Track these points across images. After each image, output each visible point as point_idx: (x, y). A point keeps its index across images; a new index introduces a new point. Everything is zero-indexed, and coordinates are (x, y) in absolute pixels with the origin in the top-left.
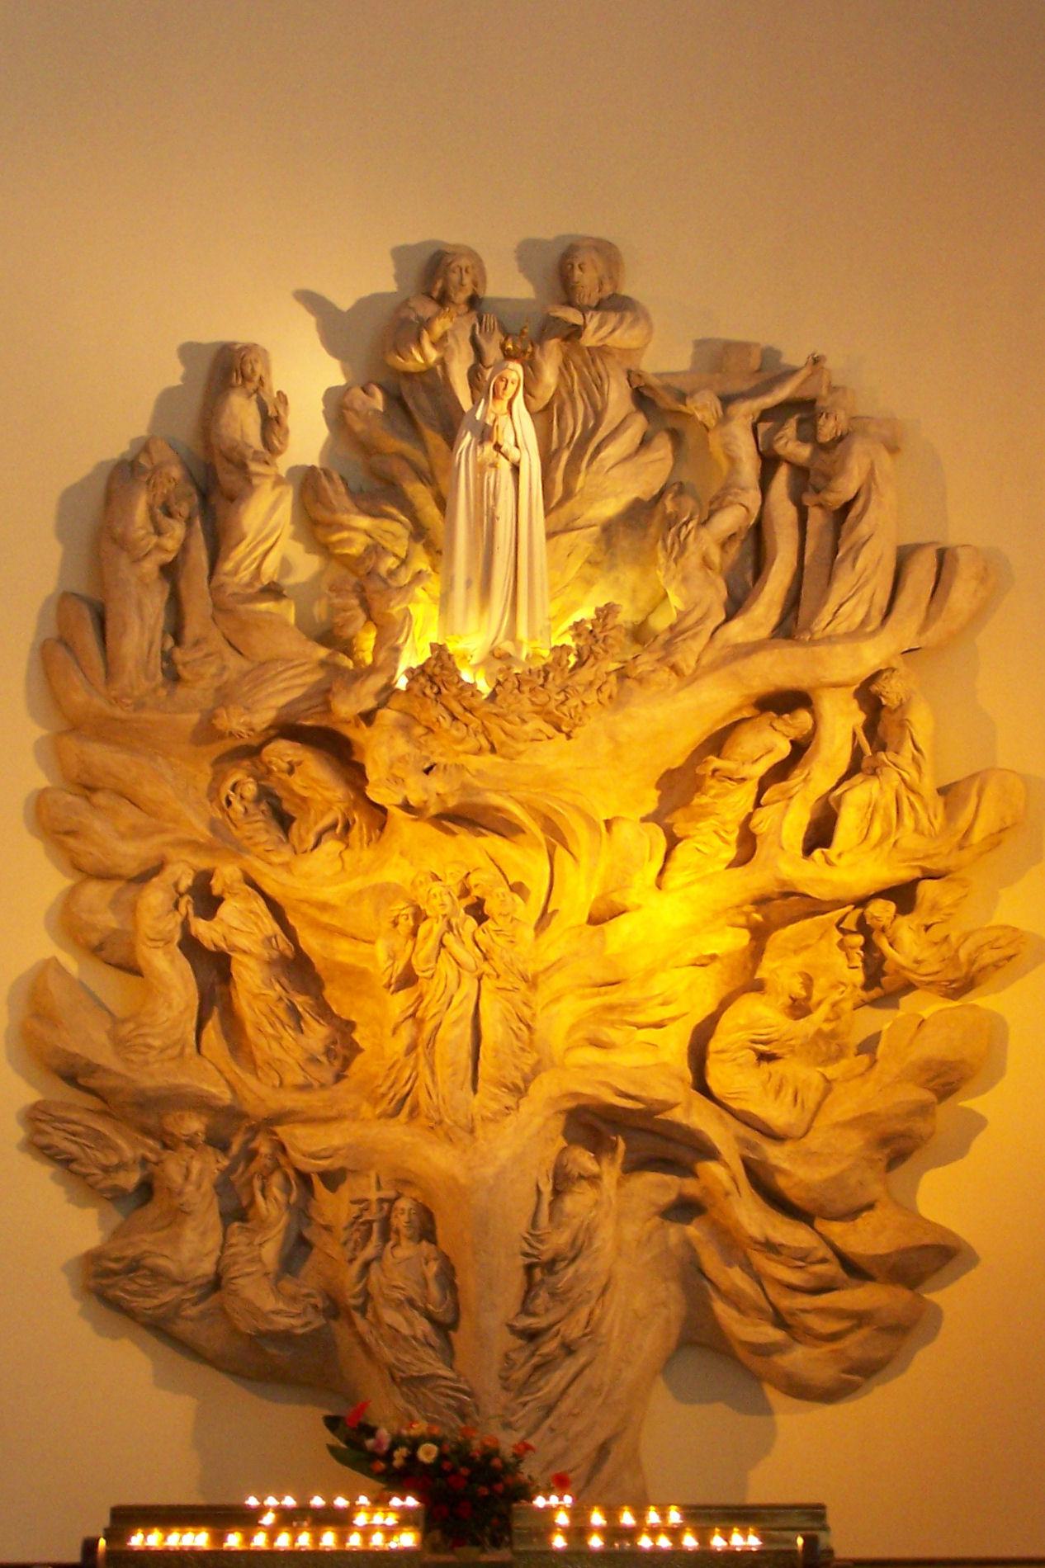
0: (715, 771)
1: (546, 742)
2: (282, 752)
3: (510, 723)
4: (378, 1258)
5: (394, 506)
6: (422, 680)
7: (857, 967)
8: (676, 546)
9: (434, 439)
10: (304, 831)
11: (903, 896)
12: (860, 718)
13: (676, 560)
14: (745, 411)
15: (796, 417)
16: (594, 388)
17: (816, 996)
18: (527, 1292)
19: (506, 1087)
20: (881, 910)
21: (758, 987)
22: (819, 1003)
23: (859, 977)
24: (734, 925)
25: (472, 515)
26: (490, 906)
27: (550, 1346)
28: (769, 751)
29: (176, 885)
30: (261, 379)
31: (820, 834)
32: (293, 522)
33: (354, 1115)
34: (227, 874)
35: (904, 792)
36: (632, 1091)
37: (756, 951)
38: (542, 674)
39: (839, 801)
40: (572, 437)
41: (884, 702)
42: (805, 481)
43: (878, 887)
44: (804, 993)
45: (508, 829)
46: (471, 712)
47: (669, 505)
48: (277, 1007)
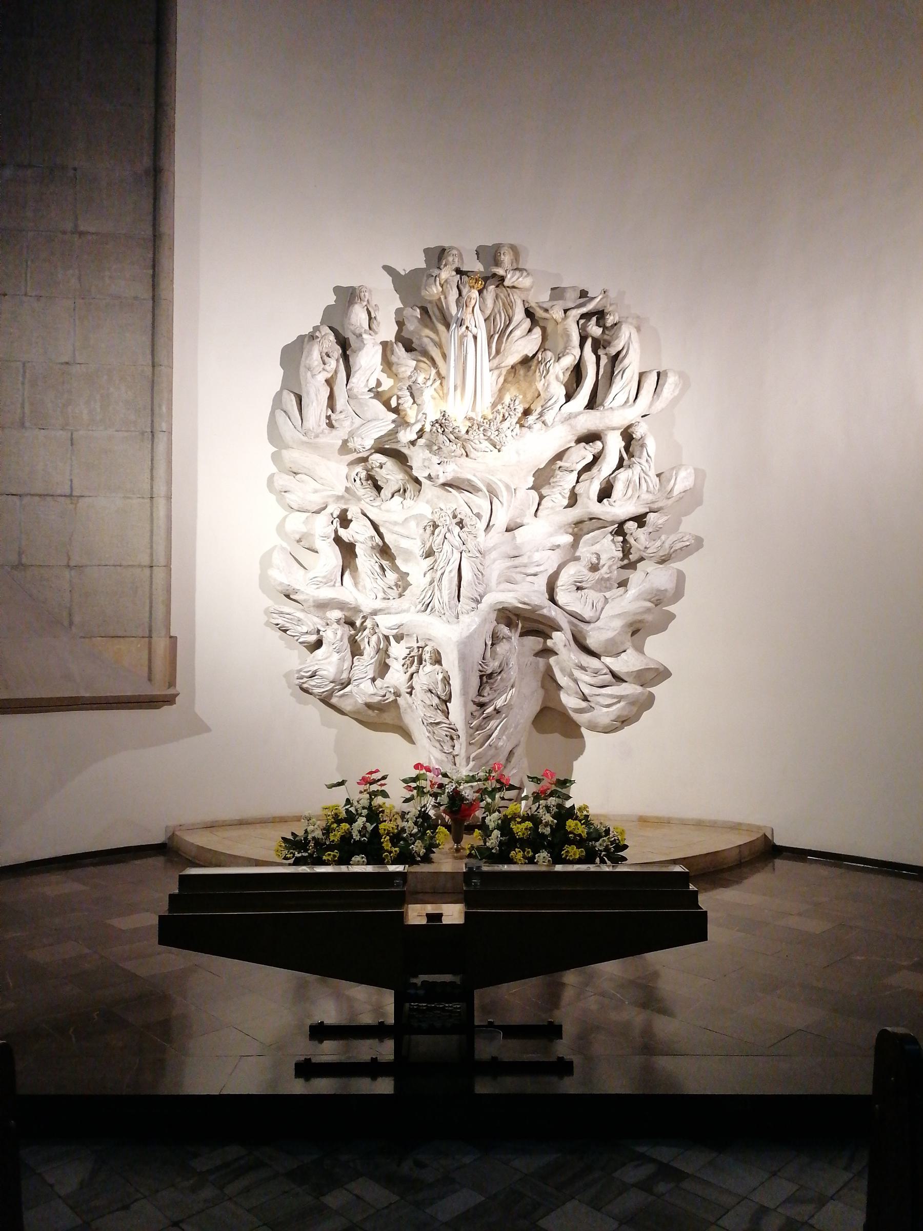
0: (560, 467)
2: (378, 458)
6: (437, 425)
8: (545, 372)
9: (441, 328)
11: (640, 520)
12: (623, 444)
14: (576, 313)
15: (596, 316)
16: (509, 306)
17: (602, 562)
19: (472, 599)
20: (631, 526)
21: (577, 559)
22: (604, 565)
23: (620, 555)
24: (567, 533)
26: (466, 521)
27: (490, 710)
29: (332, 514)
31: (605, 493)
33: (407, 611)
35: (643, 475)
36: (526, 600)
37: (575, 545)
38: (488, 423)
40: (499, 329)
41: (634, 436)
42: (597, 345)
44: (597, 562)
46: (457, 439)
47: (540, 355)
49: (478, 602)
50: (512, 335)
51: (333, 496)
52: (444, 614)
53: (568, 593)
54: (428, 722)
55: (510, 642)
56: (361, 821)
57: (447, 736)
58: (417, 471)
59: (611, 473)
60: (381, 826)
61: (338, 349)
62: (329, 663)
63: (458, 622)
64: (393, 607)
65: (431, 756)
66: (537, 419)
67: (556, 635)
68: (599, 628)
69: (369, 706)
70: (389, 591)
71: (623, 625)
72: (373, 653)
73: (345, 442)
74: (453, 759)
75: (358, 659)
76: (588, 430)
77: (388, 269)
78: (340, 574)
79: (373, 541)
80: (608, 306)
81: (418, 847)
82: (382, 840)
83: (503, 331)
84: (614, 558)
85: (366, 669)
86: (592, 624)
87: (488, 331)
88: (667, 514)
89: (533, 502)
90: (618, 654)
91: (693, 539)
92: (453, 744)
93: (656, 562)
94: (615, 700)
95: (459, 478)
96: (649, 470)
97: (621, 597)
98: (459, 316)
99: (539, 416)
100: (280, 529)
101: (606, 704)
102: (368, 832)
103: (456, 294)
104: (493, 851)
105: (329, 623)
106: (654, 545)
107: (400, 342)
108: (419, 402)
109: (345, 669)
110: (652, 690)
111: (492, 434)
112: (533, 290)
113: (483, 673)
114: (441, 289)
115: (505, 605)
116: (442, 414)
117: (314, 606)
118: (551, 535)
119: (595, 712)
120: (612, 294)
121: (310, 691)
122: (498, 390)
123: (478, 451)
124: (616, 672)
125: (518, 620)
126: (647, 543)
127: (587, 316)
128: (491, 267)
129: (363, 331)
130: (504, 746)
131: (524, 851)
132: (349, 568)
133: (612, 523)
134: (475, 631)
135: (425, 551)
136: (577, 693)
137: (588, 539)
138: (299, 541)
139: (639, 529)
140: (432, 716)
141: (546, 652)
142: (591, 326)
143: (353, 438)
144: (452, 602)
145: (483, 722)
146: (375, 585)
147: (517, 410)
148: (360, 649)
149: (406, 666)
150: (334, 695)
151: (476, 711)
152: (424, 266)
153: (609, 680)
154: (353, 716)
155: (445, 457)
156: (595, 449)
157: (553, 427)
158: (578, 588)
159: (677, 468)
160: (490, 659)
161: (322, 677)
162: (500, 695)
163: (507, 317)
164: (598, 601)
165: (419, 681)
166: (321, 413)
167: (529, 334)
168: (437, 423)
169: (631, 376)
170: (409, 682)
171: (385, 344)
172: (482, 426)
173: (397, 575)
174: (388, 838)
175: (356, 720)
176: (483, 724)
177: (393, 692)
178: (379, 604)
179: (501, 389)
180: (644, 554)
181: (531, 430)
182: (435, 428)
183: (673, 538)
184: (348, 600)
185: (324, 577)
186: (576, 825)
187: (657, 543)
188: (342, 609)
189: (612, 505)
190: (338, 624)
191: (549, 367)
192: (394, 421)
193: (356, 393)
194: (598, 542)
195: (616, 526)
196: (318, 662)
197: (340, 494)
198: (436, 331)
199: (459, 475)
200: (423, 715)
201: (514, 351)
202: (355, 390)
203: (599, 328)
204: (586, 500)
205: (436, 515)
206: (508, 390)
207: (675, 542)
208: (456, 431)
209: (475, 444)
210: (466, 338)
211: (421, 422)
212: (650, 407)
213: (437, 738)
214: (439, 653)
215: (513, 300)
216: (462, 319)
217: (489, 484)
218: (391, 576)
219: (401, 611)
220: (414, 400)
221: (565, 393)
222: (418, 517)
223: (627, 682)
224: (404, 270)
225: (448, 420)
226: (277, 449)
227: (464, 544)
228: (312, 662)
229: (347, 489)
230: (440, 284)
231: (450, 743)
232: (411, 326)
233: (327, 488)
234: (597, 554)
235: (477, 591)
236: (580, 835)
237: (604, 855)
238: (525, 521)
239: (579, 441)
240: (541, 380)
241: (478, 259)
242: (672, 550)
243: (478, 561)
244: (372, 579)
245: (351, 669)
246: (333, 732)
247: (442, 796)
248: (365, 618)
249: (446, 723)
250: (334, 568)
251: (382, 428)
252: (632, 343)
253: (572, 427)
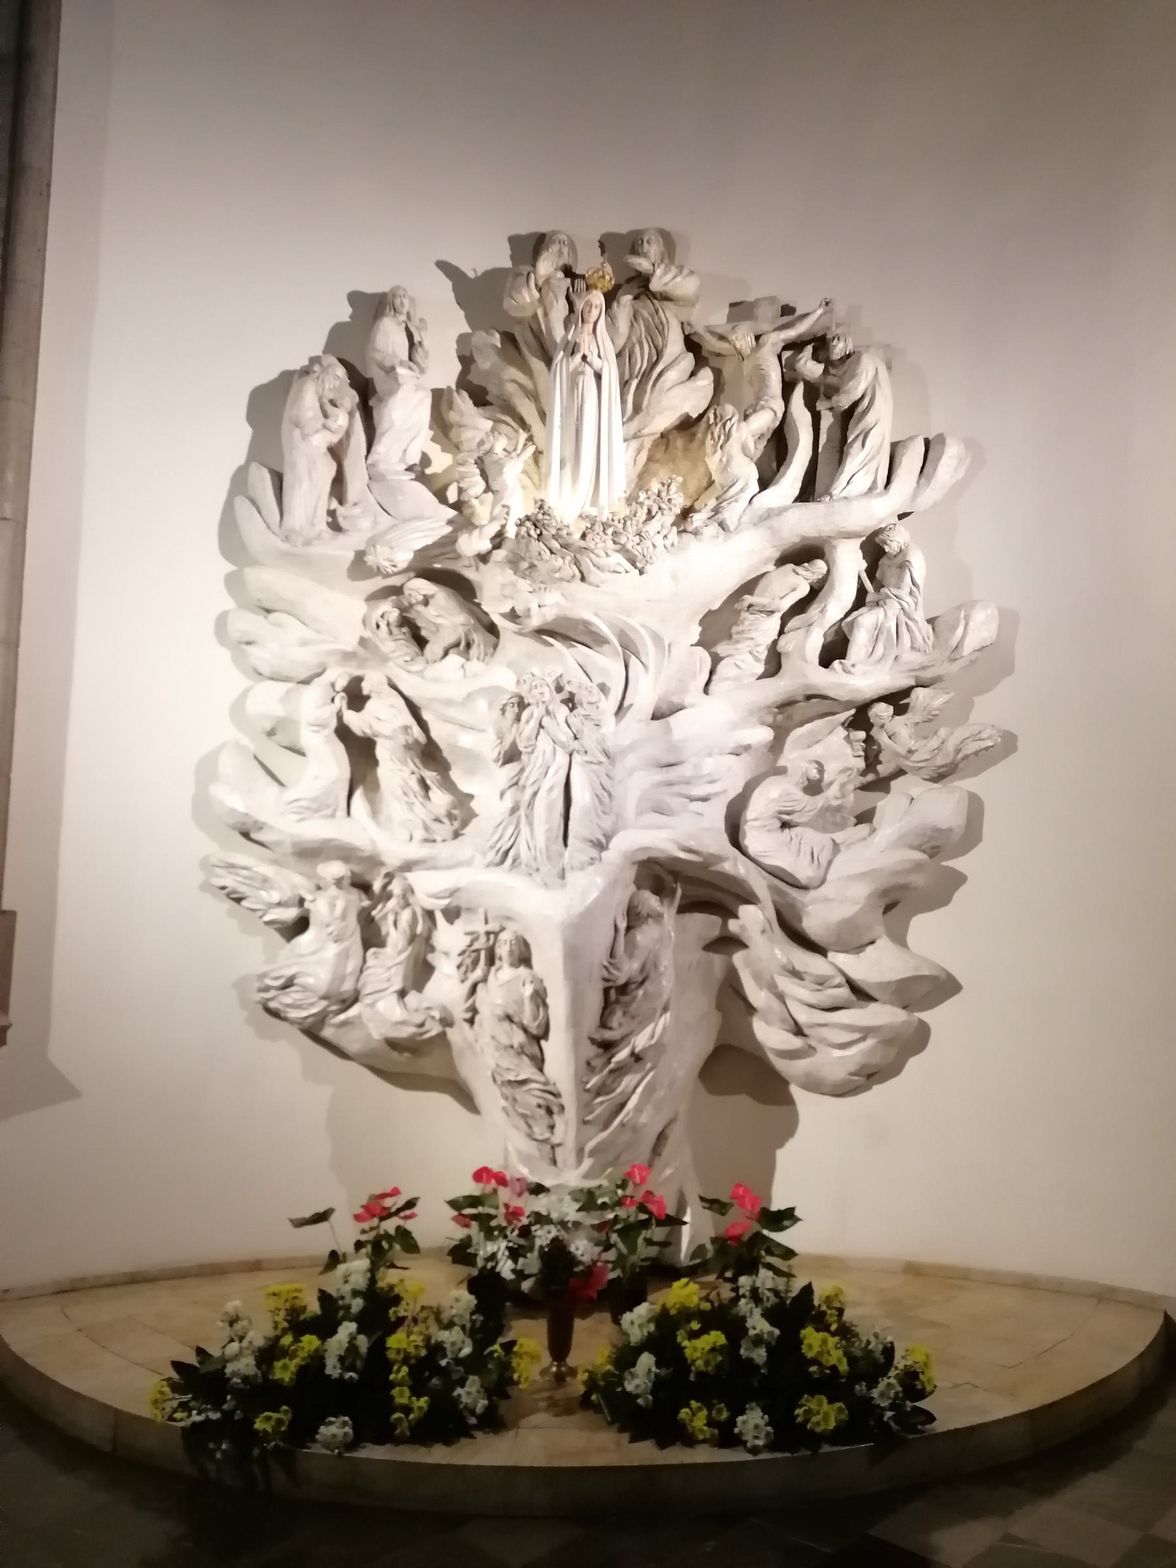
0: (750, 606)
1: (624, 574)
2: (423, 586)
3: (598, 556)
4: (484, 980)
5: (509, 415)
7: (860, 756)
8: (722, 437)
9: (537, 365)
10: (434, 648)
11: (898, 700)
12: (864, 565)
13: (721, 447)
16: (657, 331)
17: (827, 777)
18: (605, 1008)
20: (882, 711)
21: (782, 771)
22: (831, 783)
23: (861, 764)
24: (763, 723)
25: (565, 404)
26: (581, 696)
27: (622, 1055)
28: (794, 590)
29: (333, 685)
30: (408, 314)
32: (431, 428)
33: (468, 863)
35: (903, 618)
36: (692, 844)
37: (776, 747)
38: (622, 521)
39: (852, 625)
41: (887, 549)
43: (882, 692)
45: (593, 639)
46: (566, 548)
49: (601, 846)
50: (663, 379)
52: (538, 870)
56: (347, 1329)
57: (539, 1106)
59: (842, 616)
63: (564, 886)
68: (827, 900)
70: (435, 826)
73: (360, 556)
76: (803, 538)
77: (444, 266)
82: (392, 1377)
89: (701, 668)
91: (1001, 736)
92: (551, 1122)
94: (856, 1036)
96: (916, 610)
98: (570, 337)
99: (713, 513)
110: (925, 1016)
111: (631, 542)
112: (697, 306)
113: (610, 984)
115: (654, 854)
116: (538, 505)
120: (840, 310)
122: (636, 475)
124: (859, 982)
127: (795, 346)
131: (710, 1410)
133: (847, 705)
134: (596, 902)
135: (503, 752)
136: (783, 1021)
137: (801, 736)
138: (271, 733)
139: (897, 718)
141: (728, 943)
142: (804, 359)
143: (374, 546)
146: (409, 816)
147: (673, 501)
149: (463, 969)
152: (508, 264)
155: (542, 582)
156: (813, 573)
157: (738, 533)
158: (785, 825)
159: (966, 607)
161: (305, 989)
162: (642, 1025)
164: (822, 849)
167: (693, 378)
169: (879, 444)
174: (405, 1369)
178: (415, 851)
180: (908, 763)
183: (960, 733)
185: (313, 800)
186: (824, 1342)
192: (450, 522)
195: (853, 711)
197: (350, 648)
198: (528, 371)
206: (655, 475)
207: (966, 741)
208: (564, 532)
213: (521, 1110)
214: (526, 945)
218: (440, 799)
220: (487, 482)
221: (758, 477)
222: (491, 692)
224: (475, 270)
225: (549, 515)
227: (576, 738)
229: (363, 642)
230: (536, 285)
231: (546, 1121)
232: (485, 362)
234: (818, 763)
236: (834, 1368)
237: (890, 1418)
238: (687, 700)
239: (781, 561)
240: (715, 452)
242: (960, 756)
243: (602, 770)
248: (390, 876)
252: (879, 385)
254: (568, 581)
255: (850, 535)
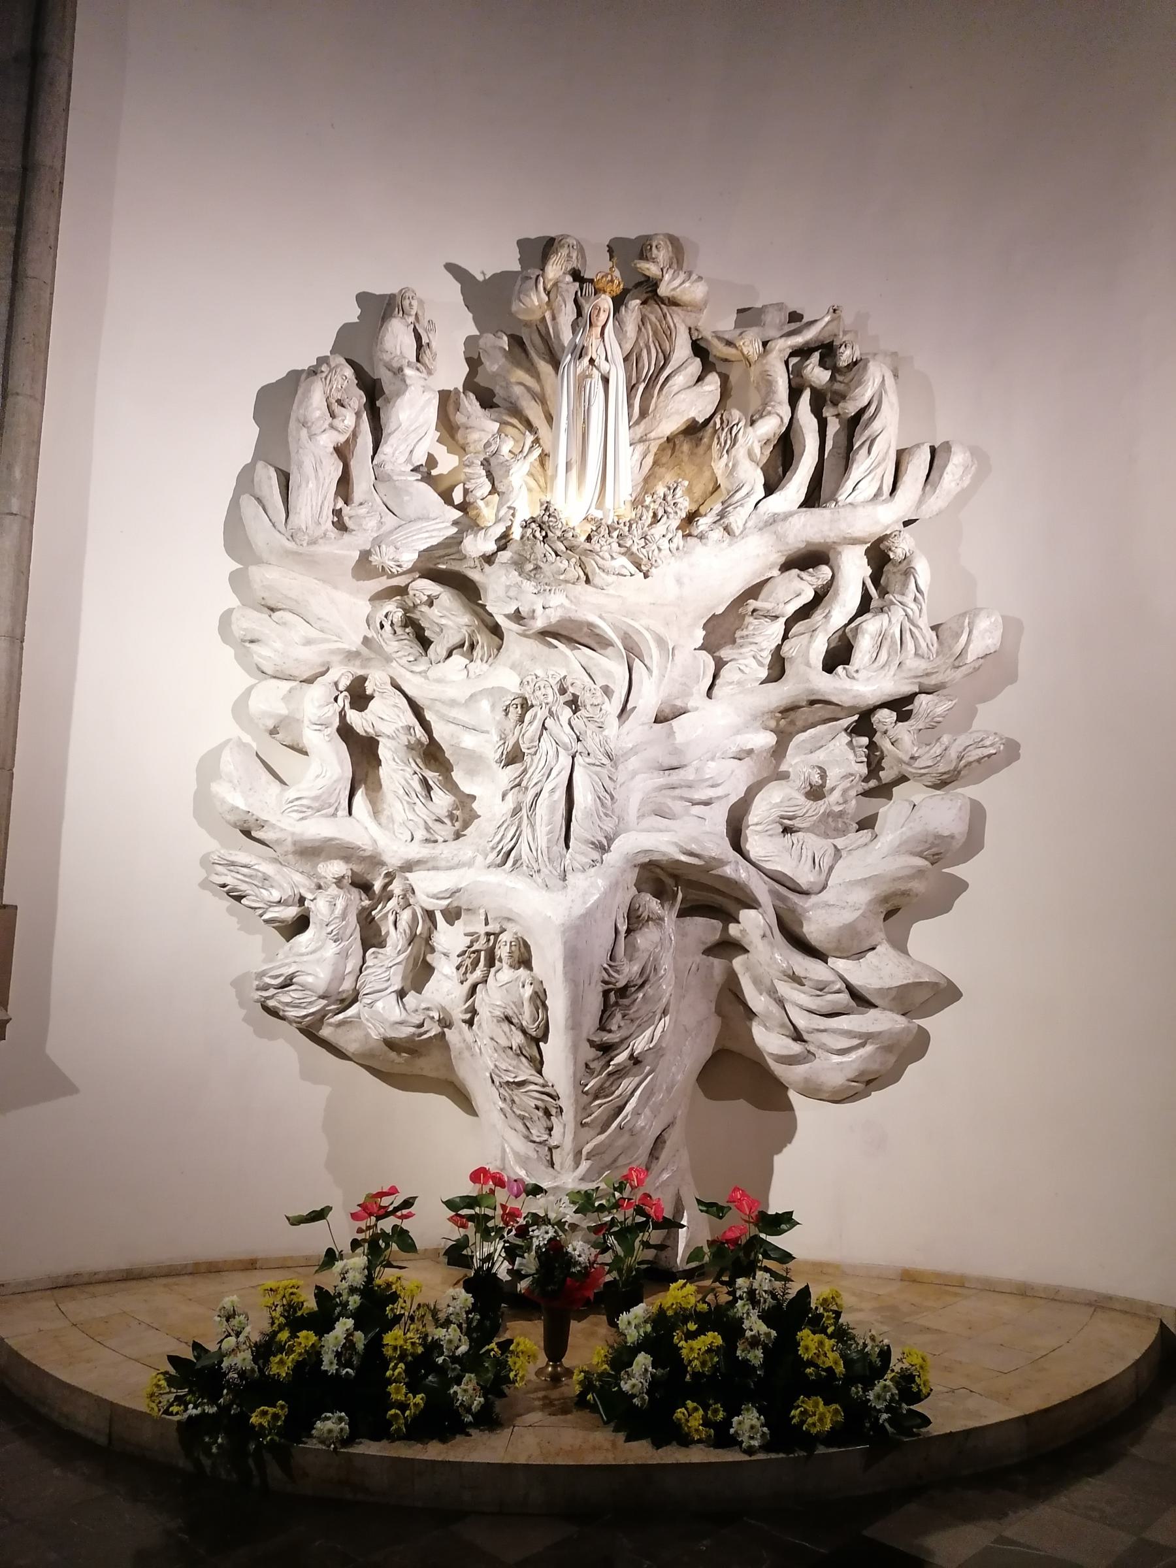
0: (754, 611)
2: (425, 587)
3: (603, 558)
8: (729, 442)
9: (544, 367)
10: (438, 649)
11: (901, 706)
12: (869, 571)
16: (665, 336)
17: (829, 784)
19: (593, 843)
20: (885, 717)
21: (785, 776)
22: (833, 789)
23: (864, 770)
24: (766, 728)
26: (585, 698)
27: (621, 1058)
29: (336, 684)
33: (470, 864)
34: (376, 681)
35: (907, 625)
36: (694, 847)
37: (779, 751)
38: (628, 524)
44: (820, 782)
48: (413, 779)
49: (603, 849)
51: (338, 651)
52: (539, 871)
53: (769, 838)
54: (501, 1080)
55: (661, 926)
56: (344, 1325)
57: (537, 1108)
58: (494, 604)
60: (389, 1338)
61: (361, 397)
62: (319, 961)
63: (565, 887)
64: (443, 856)
65: (506, 1146)
66: (715, 523)
67: (746, 915)
69: (390, 1044)
70: (437, 827)
71: (870, 901)
72: (402, 943)
73: (365, 555)
74: (549, 1154)
75: (373, 953)
76: (808, 544)
77: (454, 270)
78: (347, 793)
79: (411, 735)
80: (841, 334)
81: (467, 1391)
82: (388, 1373)
83: (653, 378)
84: (852, 775)
85: (388, 973)
86: (813, 896)
87: (629, 379)
88: (951, 698)
90: (860, 955)
92: (550, 1126)
93: (930, 784)
94: (856, 1042)
95: (571, 621)
97: (865, 849)
98: (577, 340)
99: (719, 517)
100: (240, 709)
101: (839, 1048)
102: (357, 1353)
103: (573, 313)
104: (635, 1400)
105: (322, 884)
106: (928, 752)
107: (472, 392)
108: (501, 487)
109: (349, 973)
110: (921, 1022)
111: (636, 545)
113: (611, 986)
114: (546, 299)
115: (655, 857)
116: (544, 507)
117: (295, 853)
118: (738, 732)
119: (816, 1064)
120: (848, 318)
121: (281, 1013)
123: (608, 573)
125: (677, 886)
126: (915, 749)
127: (803, 352)
128: (636, 261)
129: (405, 362)
130: (647, 1127)
131: (706, 1408)
132: (365, 784)
133: (851, 711)
134: (597, 905)
135: (505, 753)
136: (783, 1026)
138: (273, 732)
140: (511, 1068)
141: (729, 947)
142: (811, 366)
143: (379, 547)
144: (555, 848)
145: (607, 1080)
148: (380, 935)
149: (463, 969)
150: (326, 1021)
151: (593, 1060)
153: (845, 1002)
154: (360, 1062)
155: (546, 584)
158: (787, 830)
159: (970, 614)
160: (625, 961)
161: (304, 989)
162: (641, 1028)
163: (661, 355)
164: (824, 855)
165: (486, 998)
166: (323, 502)
167: (700, 383)
168: (534, 522)
170: (467, 1001)
171: (445, 398)
172: (616, 529)
173: (453, 798)
175: (369, 1068)
176: (608, 1083)
177: (437, 1017)
178: (416, 851)
179: (649, 477)
180: (910, 769)
181: (703, 541)
182: (529, 531)
183: (963, 740)
184: (359, 843)
185: (316, 798)
186: (821, 1343)
187: (934, 749)
188: (347, 859)
189: (853, 678)
190: (339, 887)
191: (736, 435)
193: (389, 472)
194: (822, 746)
195: (856, 717)
196: (297, 959)
199: (571, 615)
200: (492, 1067)
201: (673, 410)
202: (388, 467)
203: (826, 372)
204: (803, 668)
205: (528, 688)
209: (603, 559)
210: (589, 380)
211: (505, 521)
212: (921, 502)
213: (518, 1112)
214: (527, 946)
215: (672, 325)
216: (584, 346)
217: (625, 633)
218: (442, 800)
219: (458, 865)
220: (493, 485)
222: (494, 693)
223: (876, 1007)
224: (483, 273)
225: (555, 517)
226: (240, 566)
228: (287, 957)
229: (366, 641)
230: (545, 289)
231: (544, 1122)
232: (492, 365)
233: (330, 637)
234: (820, 768)
235: (601, 828)
237: (885, 1420)
239: (786, 567)
241: (610, 260)
242: (963, 763)
243: (604, 772)
244: (405, 803)
245: (361, 972)
246: (324, 1091)
247: (526, 1255)
248: (391, 877)
249: (536, 1084)
250: (335, 781)
251: (434, 534)
252: (886, 392)
253: (779, 537)
254: (574, 583)
255: (855, 541)
